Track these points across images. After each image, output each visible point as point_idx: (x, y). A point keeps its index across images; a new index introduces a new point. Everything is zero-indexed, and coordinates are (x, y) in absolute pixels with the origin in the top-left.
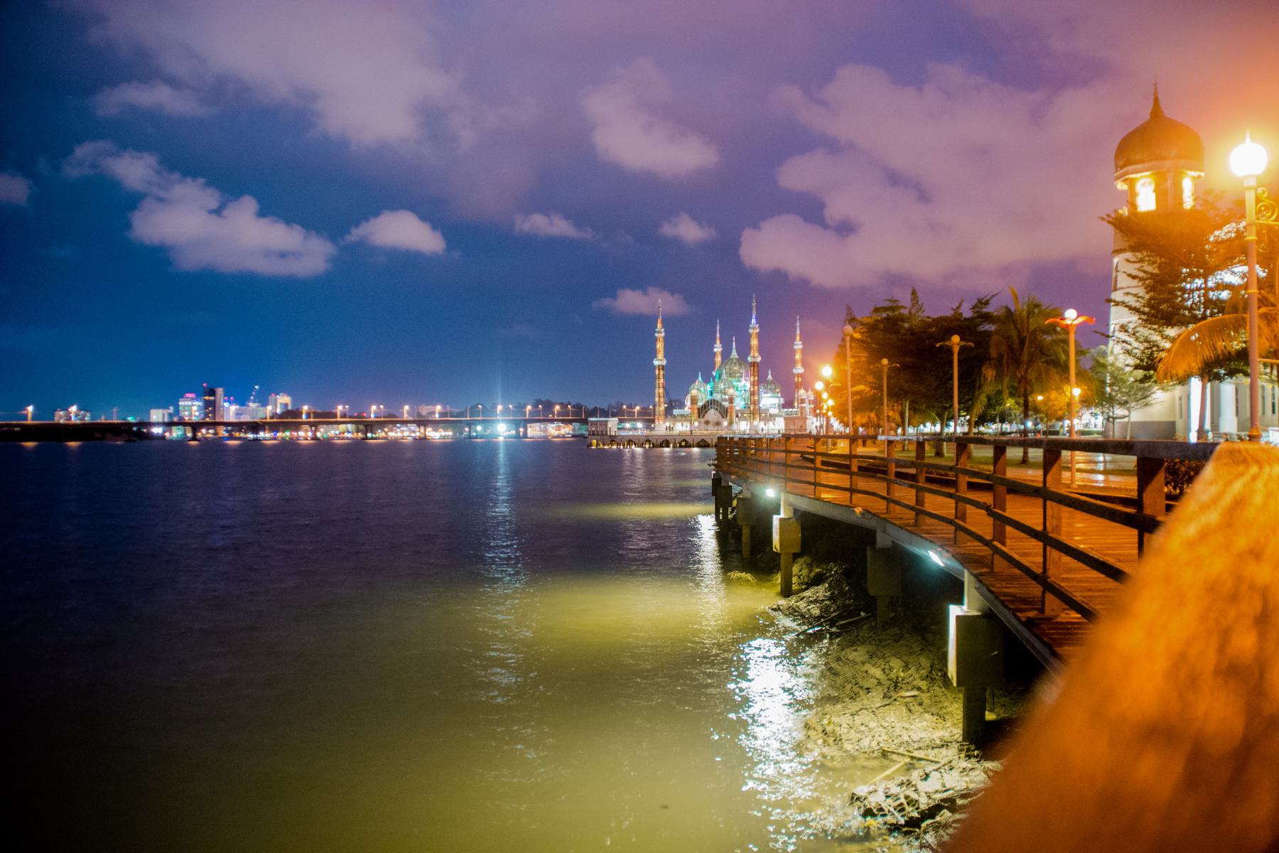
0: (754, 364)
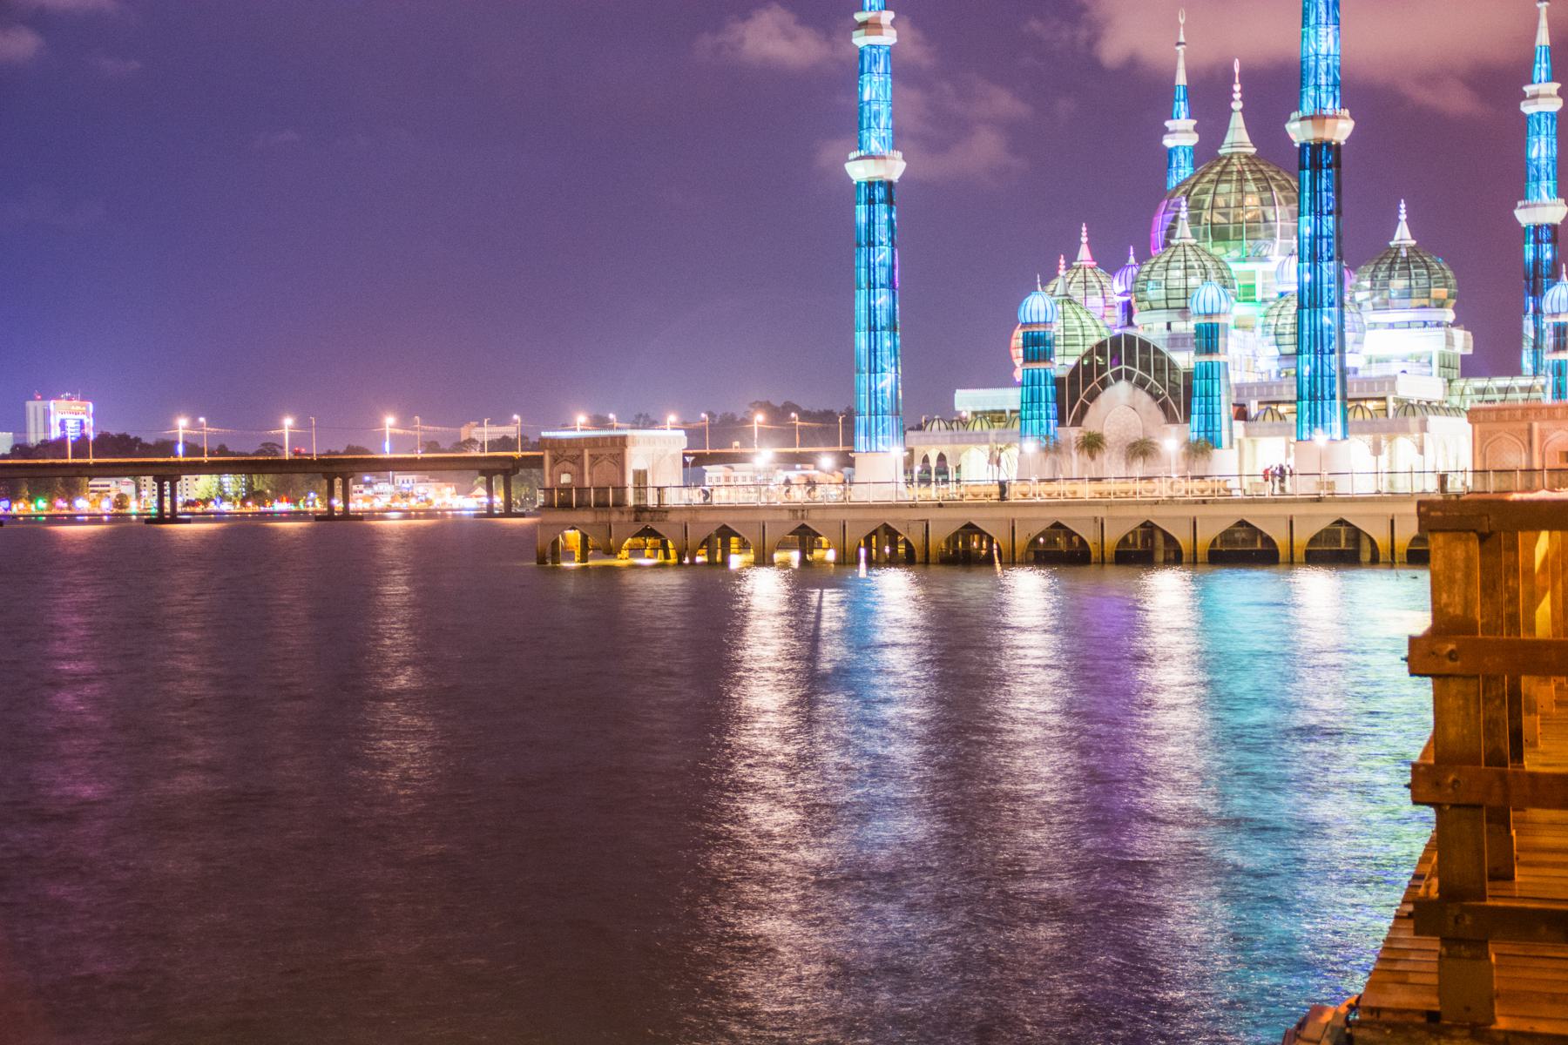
0: (1318, 156)
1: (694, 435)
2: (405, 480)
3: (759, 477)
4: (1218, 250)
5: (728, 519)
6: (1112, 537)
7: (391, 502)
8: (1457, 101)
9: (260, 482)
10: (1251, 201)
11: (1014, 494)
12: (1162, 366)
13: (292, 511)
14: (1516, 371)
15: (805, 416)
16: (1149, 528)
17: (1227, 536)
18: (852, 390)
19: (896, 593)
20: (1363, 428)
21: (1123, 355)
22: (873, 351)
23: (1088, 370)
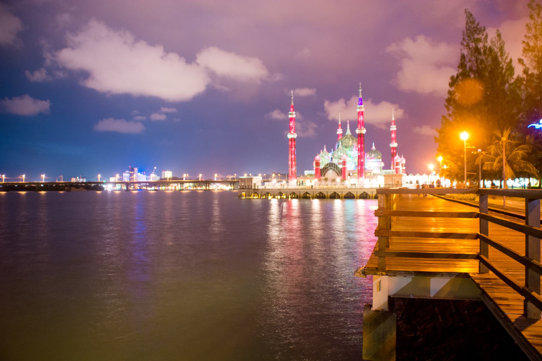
0: (360, 136)
1: (263, 178)
2: (218, 184)
3: (274, 184)
4: (346, 149)
5: (268, 191)
6: (329, 194)
7: (216, 188)
8: (383, 127)
9: (196, 184)
10: (351, 142)
11: (314, 187)
12: (337, 167)
13: (201, 189)
14: (390, 169)
15: (281, 175)
16: (335, 193)
17: (347, 194)
18: (288, 170)
19: (295, 203)
20: (368, 177)
21: (331, 165)
22: (292, 164)
23: (326, 168)
